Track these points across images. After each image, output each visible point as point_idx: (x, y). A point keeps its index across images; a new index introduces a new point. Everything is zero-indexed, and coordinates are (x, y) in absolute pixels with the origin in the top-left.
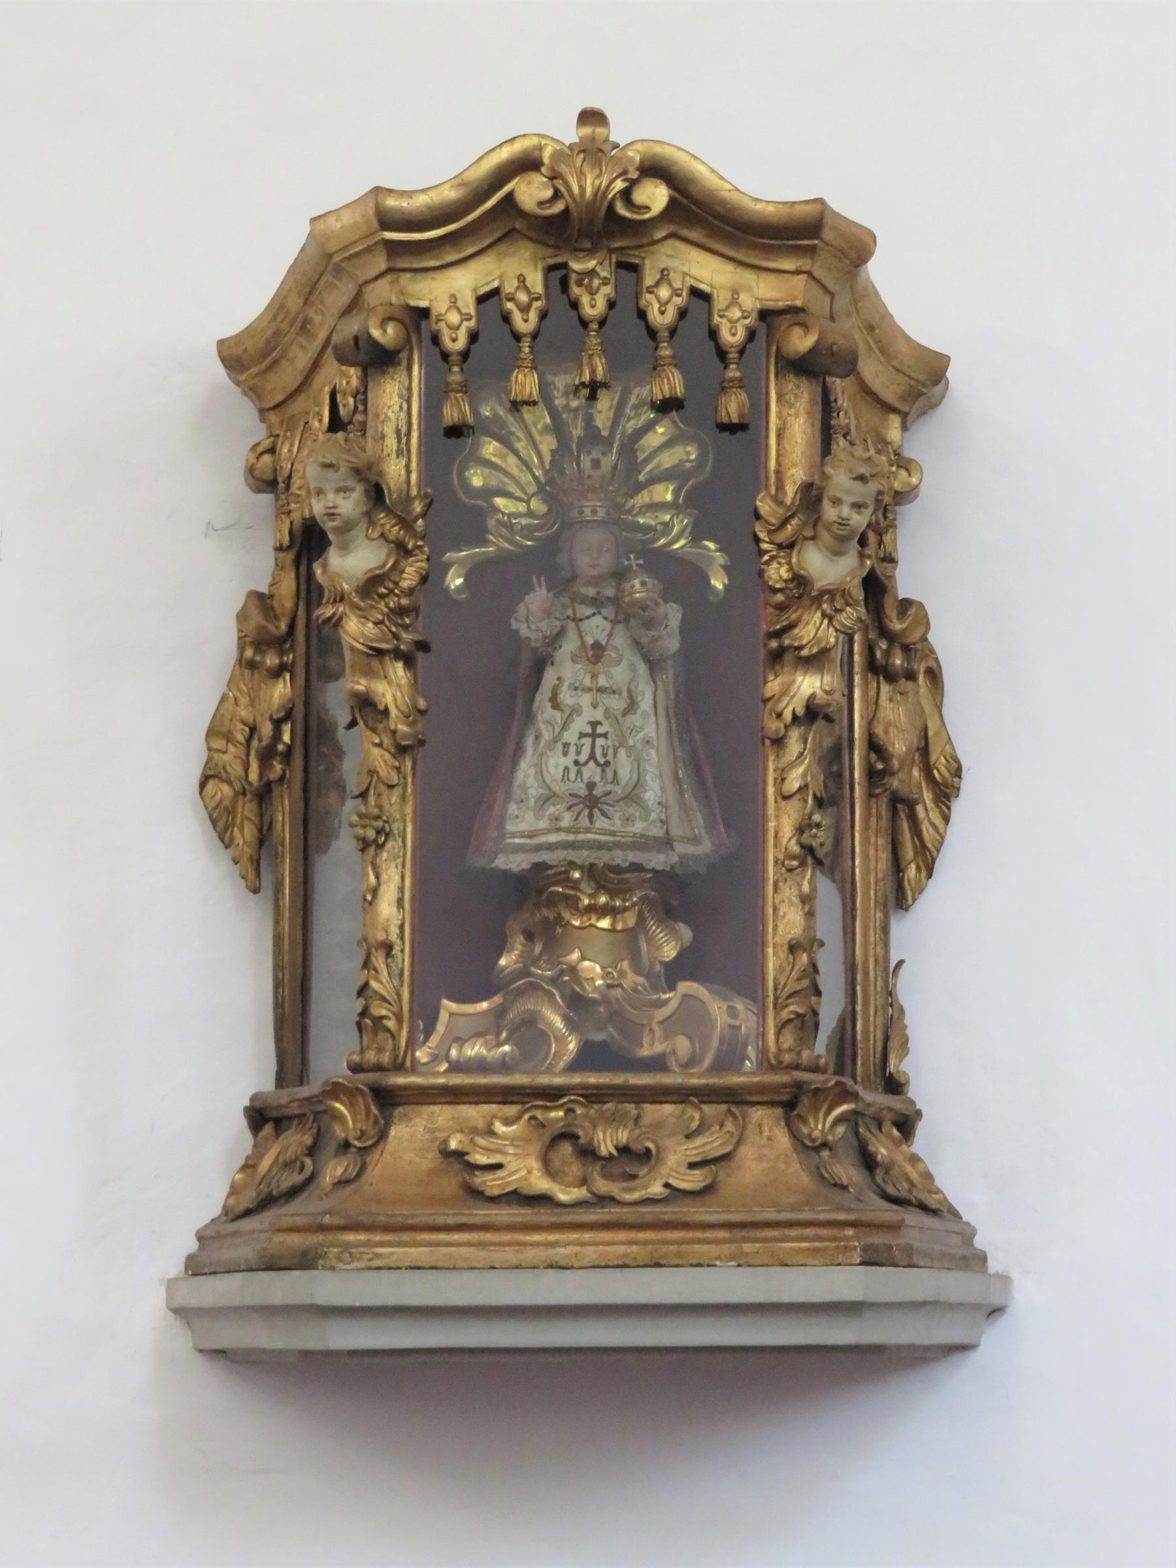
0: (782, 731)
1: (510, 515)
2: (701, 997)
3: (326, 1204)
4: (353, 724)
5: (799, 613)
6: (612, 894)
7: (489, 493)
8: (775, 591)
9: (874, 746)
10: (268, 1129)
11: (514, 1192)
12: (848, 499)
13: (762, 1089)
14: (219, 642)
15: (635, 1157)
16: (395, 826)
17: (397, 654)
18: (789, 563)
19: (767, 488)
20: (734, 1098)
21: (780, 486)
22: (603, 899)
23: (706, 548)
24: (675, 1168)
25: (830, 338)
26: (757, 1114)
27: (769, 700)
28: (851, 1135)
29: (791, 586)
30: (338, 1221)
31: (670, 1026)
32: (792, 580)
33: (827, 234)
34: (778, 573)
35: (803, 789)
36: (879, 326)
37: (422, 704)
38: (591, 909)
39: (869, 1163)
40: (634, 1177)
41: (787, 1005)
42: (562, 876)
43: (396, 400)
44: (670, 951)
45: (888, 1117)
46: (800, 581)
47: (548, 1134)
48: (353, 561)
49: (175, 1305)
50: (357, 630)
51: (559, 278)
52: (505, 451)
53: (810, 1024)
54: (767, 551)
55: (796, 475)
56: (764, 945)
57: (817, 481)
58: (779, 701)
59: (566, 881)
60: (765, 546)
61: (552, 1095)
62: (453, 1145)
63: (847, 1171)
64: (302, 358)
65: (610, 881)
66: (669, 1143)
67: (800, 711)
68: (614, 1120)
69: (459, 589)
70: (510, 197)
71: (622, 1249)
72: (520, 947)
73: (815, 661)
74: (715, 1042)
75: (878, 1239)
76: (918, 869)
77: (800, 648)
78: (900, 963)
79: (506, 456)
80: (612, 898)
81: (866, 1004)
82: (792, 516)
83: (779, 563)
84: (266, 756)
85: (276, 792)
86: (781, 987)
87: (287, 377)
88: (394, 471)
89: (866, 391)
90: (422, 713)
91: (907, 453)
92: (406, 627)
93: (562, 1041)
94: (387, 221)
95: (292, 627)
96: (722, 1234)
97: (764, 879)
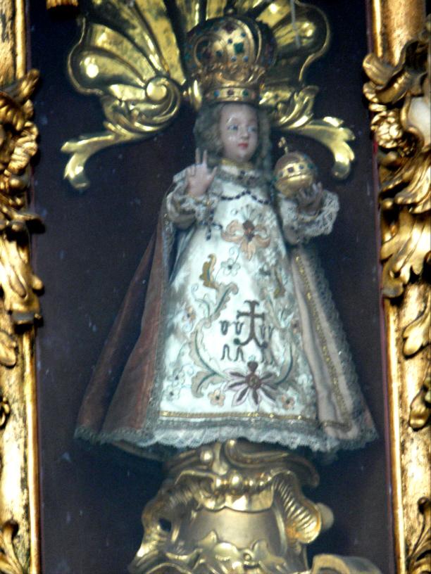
0: (401, 290)
1: (127, 102)
2: (337, 568)
5: (411, 171)
7: (104, 81)
8: (386, 151)
16: (15, 407)
18: (399, 121)
19: (374, 50)
21: (387, 47)
22: (235, 480)
23: (327, 124)
27: (386, 260)
29: (401, 144)
32: (403, 138)
34: (387, 133)
37: (37, 283)
38: (224, 490)
41: (419, 565)
42: (194, 459)
44: (312, 531)
46: (410, 139)
52: (121, 38)
54: (376, 113)
55: (401, 37)
56: (393, 507)
57: (421, 39)
58: (397, 260)
59: (198, 463)
60: (374, 107)
65: (244, 461)
69: (78, 179)
72: (156, 537)
77: (414, 205)
79: (121, 43)
80: (245, 478)
82: (399, 75)
83: (389, 123)
86: (412, 548)
90: (39, 293)
92: (18, 208)
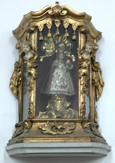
3: (24, 135)
4: (28, 76)
6: (61, 98)
7: (46, 49)
9: (93, 80)
10: (18, 127)
11: (48, 133)
12: (89, 48)
13: (78, 121)
14: (12, 67)
15: (62, 129)
17: (34, 68)
20: (75, 122)
24: (67, 131)
25: (86, 29)
26: (78, 124)
28: (89, 127)
30: (26, 137)
31: (68, 114)
33: (86, 17)
34: (80, 57)
35: (83, 84)
36: (93, 28)
39: (92, 130)
40: (62, 131)
43: (34, 36)
44: (68, 105)
45: (95, 126)
46: (83, 58)
47: (52, 127)
48: (29, 56)
49: (7, 149)
50: (29, 64)
51: (53, 22)
53: (84, 112)
55: (82, 46)
56: (79, 103)
61: (52, 121)
62: (40, 128)
63: (89, 131)
64: (23, 33)
66: (67, 127)
67: (83, 74)
68: (59, 125)
70: (47, 12)
71: (61, 140)
73: (85, 68)
74: (73, 116)
75: (92, 139)
76: (99, 96)
78: (97, 107)
81: (92, 112)
84: (18, 81)
85: (19, 86)
87: (20, 35)
88: (33, 45)
89: (92, 36)
91: (97, 44)
93: (54, 116)
94: (33, 15)
95: (21, 66)
96: (73, 138)
97: (79, 95)
